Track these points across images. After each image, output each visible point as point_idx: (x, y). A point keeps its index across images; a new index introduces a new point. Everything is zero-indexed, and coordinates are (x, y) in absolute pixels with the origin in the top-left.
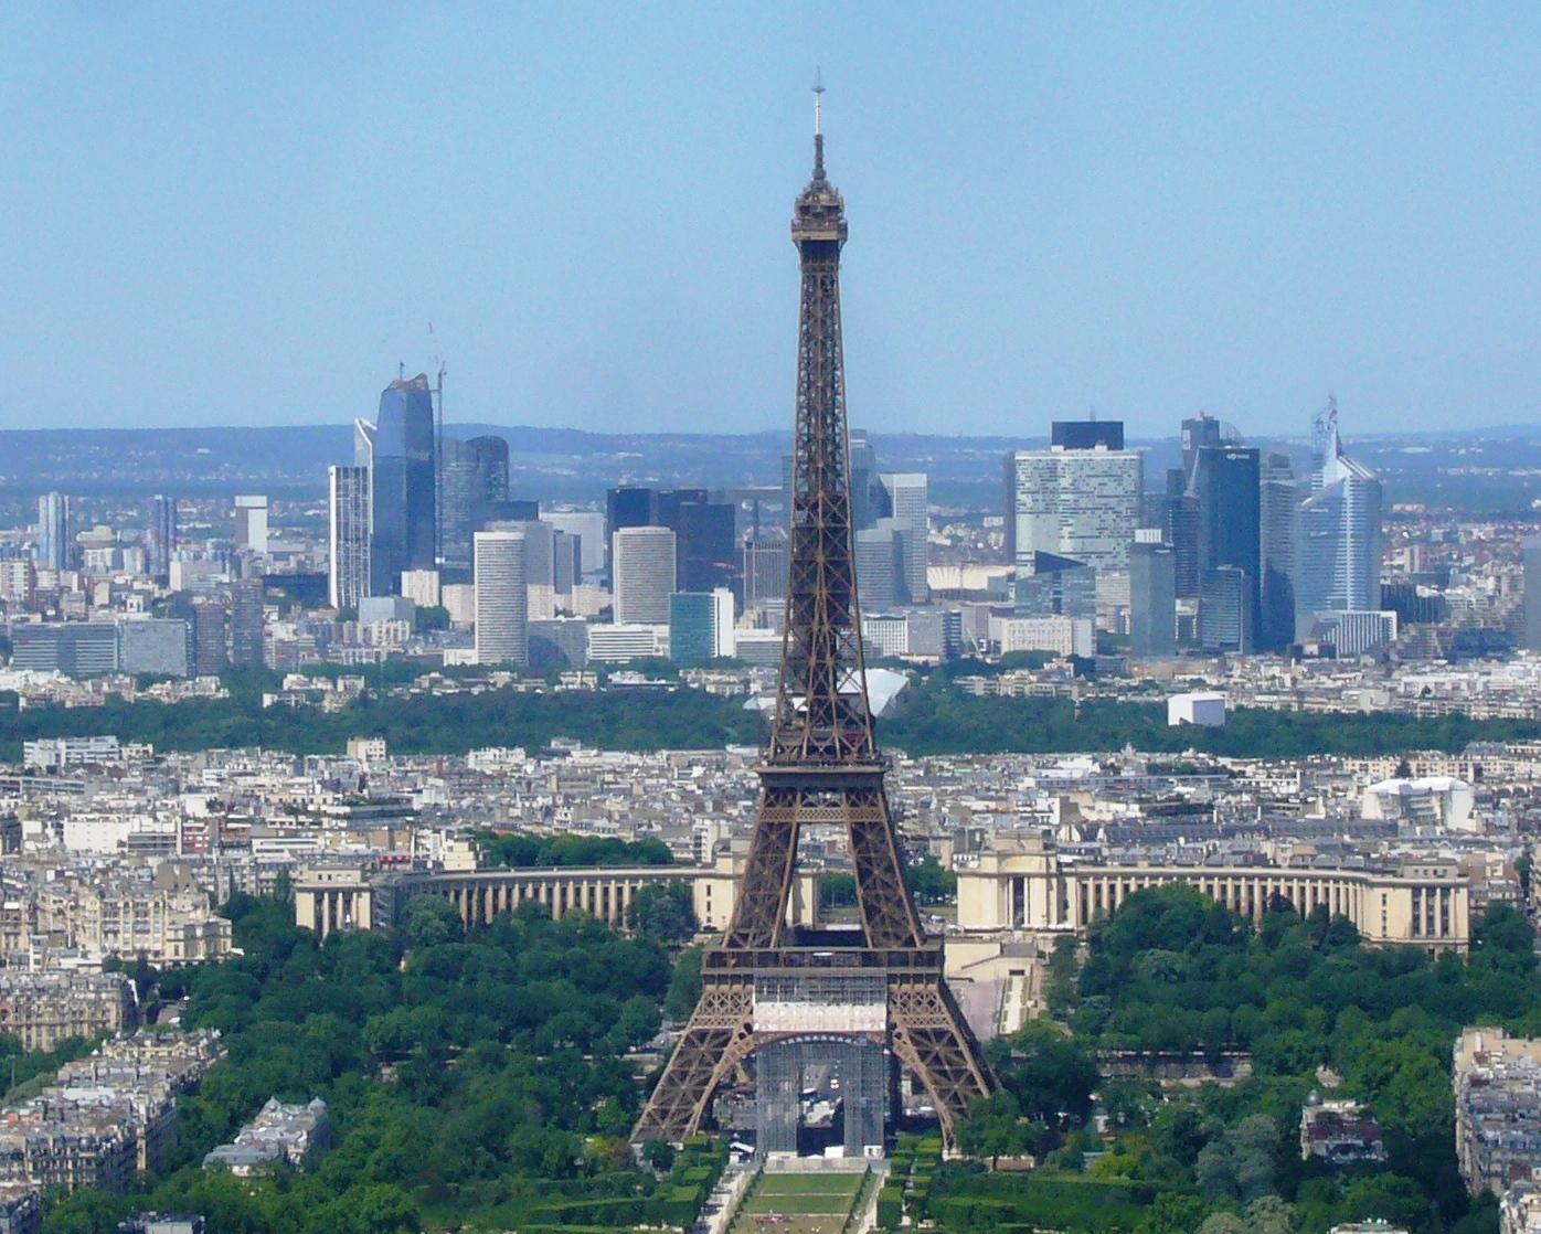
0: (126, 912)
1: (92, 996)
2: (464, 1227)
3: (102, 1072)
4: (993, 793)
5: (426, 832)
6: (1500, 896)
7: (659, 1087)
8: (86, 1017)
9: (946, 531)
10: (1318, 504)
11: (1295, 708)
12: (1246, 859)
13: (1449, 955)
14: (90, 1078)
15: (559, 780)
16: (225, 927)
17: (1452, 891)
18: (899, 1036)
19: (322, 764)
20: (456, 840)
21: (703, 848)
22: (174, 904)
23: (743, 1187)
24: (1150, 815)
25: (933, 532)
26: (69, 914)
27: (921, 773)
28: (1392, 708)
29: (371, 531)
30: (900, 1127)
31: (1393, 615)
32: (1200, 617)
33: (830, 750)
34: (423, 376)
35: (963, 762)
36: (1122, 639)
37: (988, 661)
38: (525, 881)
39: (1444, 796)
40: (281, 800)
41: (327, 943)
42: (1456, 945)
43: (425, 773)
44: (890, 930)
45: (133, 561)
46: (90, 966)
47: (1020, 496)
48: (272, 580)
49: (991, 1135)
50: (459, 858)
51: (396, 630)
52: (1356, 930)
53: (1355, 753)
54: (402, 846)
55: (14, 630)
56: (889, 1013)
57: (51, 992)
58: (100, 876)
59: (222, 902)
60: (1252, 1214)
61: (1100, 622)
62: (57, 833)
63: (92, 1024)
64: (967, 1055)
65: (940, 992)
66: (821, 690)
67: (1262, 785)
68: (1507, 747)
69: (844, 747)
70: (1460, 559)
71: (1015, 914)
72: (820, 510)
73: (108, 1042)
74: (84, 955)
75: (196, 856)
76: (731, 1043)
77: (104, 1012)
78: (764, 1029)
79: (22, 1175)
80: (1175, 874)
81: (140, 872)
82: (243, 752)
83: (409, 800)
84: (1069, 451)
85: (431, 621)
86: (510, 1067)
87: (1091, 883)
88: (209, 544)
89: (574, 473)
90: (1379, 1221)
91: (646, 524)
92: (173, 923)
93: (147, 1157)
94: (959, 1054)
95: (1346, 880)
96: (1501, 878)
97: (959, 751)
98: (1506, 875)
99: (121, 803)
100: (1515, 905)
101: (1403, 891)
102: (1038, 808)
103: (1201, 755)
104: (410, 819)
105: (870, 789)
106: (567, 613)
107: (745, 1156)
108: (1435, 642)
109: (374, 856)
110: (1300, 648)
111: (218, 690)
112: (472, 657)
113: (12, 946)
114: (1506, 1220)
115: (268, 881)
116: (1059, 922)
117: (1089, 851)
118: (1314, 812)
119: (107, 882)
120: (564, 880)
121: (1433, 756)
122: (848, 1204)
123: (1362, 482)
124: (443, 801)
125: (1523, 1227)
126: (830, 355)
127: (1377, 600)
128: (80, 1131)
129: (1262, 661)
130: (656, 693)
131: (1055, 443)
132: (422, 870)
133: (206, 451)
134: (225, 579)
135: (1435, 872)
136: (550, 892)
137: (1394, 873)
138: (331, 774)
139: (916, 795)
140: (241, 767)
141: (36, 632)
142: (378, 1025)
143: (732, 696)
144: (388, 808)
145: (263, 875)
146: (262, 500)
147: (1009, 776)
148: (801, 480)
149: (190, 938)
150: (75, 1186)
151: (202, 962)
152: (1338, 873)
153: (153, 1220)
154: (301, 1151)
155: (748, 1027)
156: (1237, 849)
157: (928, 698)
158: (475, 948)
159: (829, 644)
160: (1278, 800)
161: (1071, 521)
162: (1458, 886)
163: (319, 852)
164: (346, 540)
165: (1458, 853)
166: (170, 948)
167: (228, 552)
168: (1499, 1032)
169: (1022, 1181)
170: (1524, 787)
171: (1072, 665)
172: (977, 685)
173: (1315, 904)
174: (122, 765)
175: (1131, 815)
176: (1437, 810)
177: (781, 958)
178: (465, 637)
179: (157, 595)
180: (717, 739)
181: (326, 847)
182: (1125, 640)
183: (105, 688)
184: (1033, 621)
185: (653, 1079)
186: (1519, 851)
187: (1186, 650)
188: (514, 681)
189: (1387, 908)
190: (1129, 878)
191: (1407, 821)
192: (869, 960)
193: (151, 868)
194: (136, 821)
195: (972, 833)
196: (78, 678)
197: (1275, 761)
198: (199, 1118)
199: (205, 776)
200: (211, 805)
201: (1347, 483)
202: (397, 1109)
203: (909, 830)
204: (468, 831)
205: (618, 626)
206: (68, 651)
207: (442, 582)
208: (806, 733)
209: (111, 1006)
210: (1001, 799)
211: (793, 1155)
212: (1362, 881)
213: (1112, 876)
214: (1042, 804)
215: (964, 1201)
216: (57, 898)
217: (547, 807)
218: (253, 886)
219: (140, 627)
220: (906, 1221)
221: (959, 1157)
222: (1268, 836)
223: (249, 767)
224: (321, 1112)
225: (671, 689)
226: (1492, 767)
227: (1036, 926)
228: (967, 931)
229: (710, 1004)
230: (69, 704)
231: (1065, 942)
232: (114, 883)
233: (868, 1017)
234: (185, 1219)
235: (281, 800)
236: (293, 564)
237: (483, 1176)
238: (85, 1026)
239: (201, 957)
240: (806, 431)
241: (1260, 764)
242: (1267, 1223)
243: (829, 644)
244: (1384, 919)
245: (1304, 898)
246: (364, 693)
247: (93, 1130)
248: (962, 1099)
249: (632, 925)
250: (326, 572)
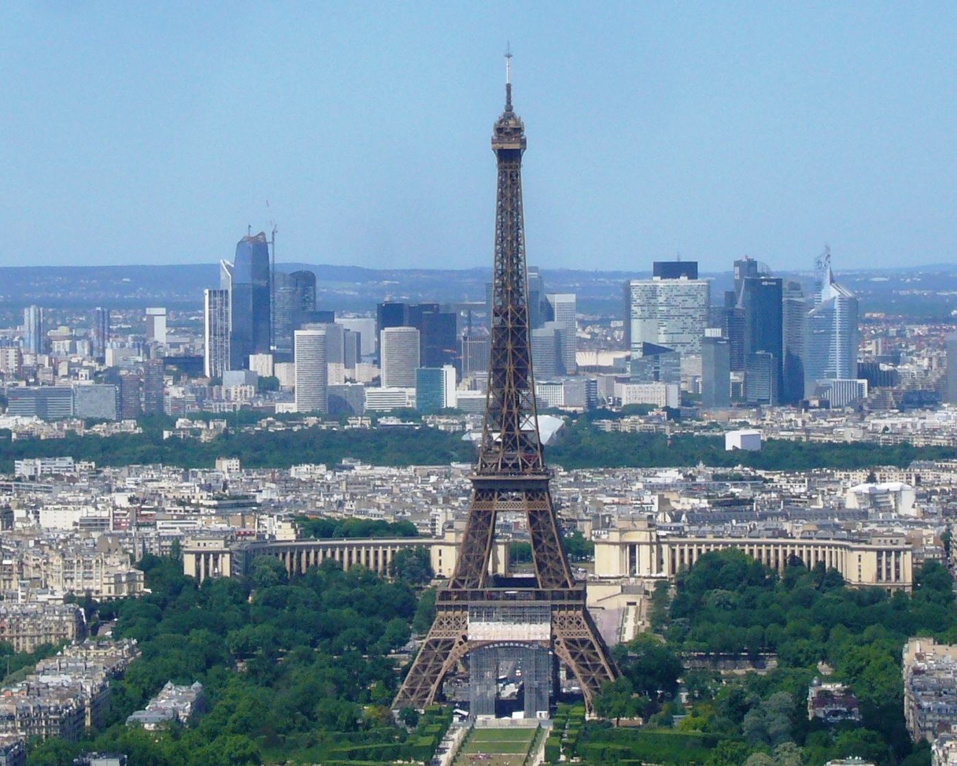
0: (78, 566)
1: (57, 618)
2: (288, 762)
3: (63, 665)
4: (616, 492)
5: (265, 517)
6: (931, 556)
7: (409, 675)
8: (53, 631)
9: (587, 330)
10: (819, 313)
11: (804, 440)
12: (774, 533)
13: (900, 593)
14: (56, 669)
15: (347, 484)
16: (140, 576)
17: (902, 553)
19: (200, 474)
20: (283, 522)
21: (437, 526)
22: (108, 561)
23: (462, 737)
25: (579, 330)
26: (43, 567)
27: (572, 480)
28: (864, 440)
29: (230, 330)
30: (559, 700)
31: (865, 382)
32: (745, 383)
33: (515, 466)
34: (262, 234)
36: (697, 396)
37: (614, 410)
38: (326, 547)
39: (897, 494)
40: (174, 497)
41: (203, 585)
42: (904, 586)
43: (264, 480)
44: (553, 577)
45: (83, 348)
46: (56, 599)
47: (633, 308)
48: (169, 360)
49: (616, 704)
50: (285, 533)
51: (246, 391)
52: (842, 578)
53: (841, 467)
54: (250, 525)
55: (8, 391)
56: (552, 629)
57: (32, 615)
58: (62, 544)
59: (138, 560)
60: (778, 753)
61: (683, 386)
62: (35, 517)
63: (57, 635)
64: (601, 655)
65: (584, 616)
66: (510, 428)
67: (784, 487)
68: (936, 464)
69: (524, 464)
71: (630, 567)
72: (509, 317)
73: (67, 647)
74: (52, 593)
75: (121, 531)
76: (454, 647)
77: (64, 628)
78: (474, 639)
79: (14, 730)
80: (730, 543)
81: (87, 541)
82: (151, 467)
83: (254, 497)
84: (664, 280)
85: (268, 385)
86: (317, 662)
87: (677, 548)
88: (130, 338)
89: (356, 293)
90: (857, 758)
91: (401, 325)
92: (107, 573)
93: (91, 718)
94: (596, 654)
95: (836, 546)
96: (932, 545)
98: (935, 543)
99: (75, 499)
100: (941, 562)
101: (871, 553)
102: (645, 502)
103: (746, 469)
104: (255, 508)
105: (540, 490)
106: (352, 380)
107: (463, 718)
108: (891, 398)
109: (232, 532)
110: (807, 402)
111: (135, 428)
112: (293, 408)
113: (7, 587)
114: (935, 757)
115: (166, 547)
116: (657, 573)
117: (677, 528)
118: (816, 504)
119: (66, 548)
120: (350, 546)
121: (890, 469)
122: (527, 747)
123: (846, 299)
124: (275, 497)
125: (946, 761)
126: (515, 220)
127: (855, 372)
128: (50, 702)
129: (784, 410)
130: (408, 430)
131: (655, 275)
132: (262, 540)
133: (128, 280)
134: (140, 359)
135: (891, 541)
136: (341, 554)
137: (866, 542)
138: (205, 481)
139: (569, 493)
140: (150, 476)
141: (23, 393)
143: (455, 432)
144: (241, 501)
145: (164, 543)
146: (163, 311)
147: (627, 482)
148: (497, 298)
149: (118, 583)
150: (47, 736)
151: (125, 597)
152: (831, 542)
153: (95, 757)
154: (187, 714)
155: (465, 638)
156: (768, 527)
157: (576, 433)
158: (295, 588)
159: (515, 400)
160: (793, 497)
161: (665, 323)
162: (905, 550)
164: (215, 335)
165: (905, 529)
166: (105, 589)
167: (142, 343)
168: (931, 641)
169: (635, 733)
170: (947, 488)
171: (666, 413)
172: (607, 425)
173: (817, 561)
174: (76, 475)
175: (702, 506)
176: (893, 503)
177: (485, 595)
178: (289, 395)
179: (97, 369)
180: (445, 459)
181: (203, 526)
182: (699, 397)
183: (65, 427)
184: (642, 386)
185: (406, 670)
186: (944, 528)
187: (737, 404)
188: (319, 423)
189: (861, 564)
190: (701, 545)
191: (874, 510)
192: (540, 596)
193: (94, 539)
194: (85, 510)
195: (604, 517)
196: (49, 421)
197: (792, 472)
198: (124, 694)
199: (127, 482)
200: (131, 500)
201: (837, 300)
203: (565, 516)
204: (291, 516)
205: (384, 388)
206: (42, 404)
207: (275, 362)
208: (501, 455)
209: (69, 624)
210: (622, 496)
211: (493, 717)
212: (846, 547)
213: (691, 544)
214: (647, 499)
215: (599, 746)
216: (35, 558)
217: (340, 501)
218: (157, 550)
219: (87, 389)
220: (563, 758)
221: (596, 718)
222: (787, 519)
223: (155, 476)
224: (200, 690)
225: (417, 428)
226: (927, 476)
227: (643, 575)
228: (600, 578)
229: (441, 623)
230: (43, 437)
231: (662, 585)
232: (71, 548)
233: (539, 631)
234: (115, 757)
235: (174, 497)
236: (182, 350)
237: (300, 730)
238: (53, 637)
239: (125, 594)
240: (500, 267)
241: (783, 474)
242: (787, 759)
244: (860, 570)
245: (810, 558)
246: (226, 430)
247: (58, 702)
248: (597, 682)
249: (392, 574)
250: (202, 355)
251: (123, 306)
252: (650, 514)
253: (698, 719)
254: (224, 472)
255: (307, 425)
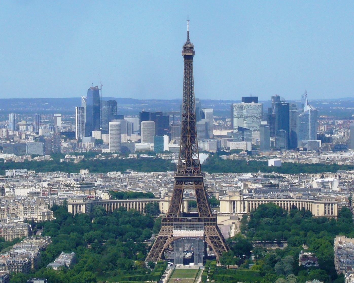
0: (29, 209)
1: (21, 228)
2: (107, 281)
3: (23, 246)
4: (228, 182)
5: (98, 191)
6: (345, 205)
7: (151, 249)
8: (20, 233)
9: (217, 122)
10: (303, 116)
11: (297, 162)
12: (286, 197)
13: (333, 219)
14: (21, 247)
15: (128, 179)
16: (52, 213)
17: (334, 204)
18: (206, 238)
19: (74, 175)
20: (105, 193)
21: (162, 194)
22: (40, 207)
23: (171, 272)
24: (264, 187)
25: (214, 122)
26: (16, 210)
27: (212, 177)
28: (320, 162)
29: (85, 122)
30: (207, 258)
31: (320, 141)
32: (276, 142)
33: (191, 172)
34: (97, 86)
35: (221, 175)
36: (258, 146)
37: (227, 152)
38: (121, 202)
39: (332, 183)
40: (64, 183)
41: (75, 216)
42: (335, 217)
43: (98, 177)
44: (204, 213)
45: (31, 129)
46: (21, 221)
47: (234, 114)
48: (63, 133)
49: (228, 260)
50: (105, 197)
51: (91, 145)
52: (312, 213)
53: (311, 173)
54: (92, 194)
55: (3, 145)
56: (204, 232)
57: (12, 227)
58: (23, 201)
59: (51, 207)
60: (288, 278)
61: (253, 143)
62: (13, 191)
63: (21, 235)
64: (222, 242)
65: (216, 227)
66: (189, 158)
67: (290, 180)
68: (346, 171)
69: (194, 171)
70: (335, 128)
71: (233, 210)
72: (188, 117)
73: (25, 239)
74: (19, 219)
75: (45, 196)
76: (168, 239)
77: (24, 232)
78: (175, 236)
79: (5, 270)
80: (270, 201)
81: (32, 200)
82: (56, 172)
83: (94, 184)
84: (246, 104)
85: (99, 142)
86: (117, 245)
87: (251, 202)
88: (48, 125)
89: (132, 108)
90: (317, 280)
91: (148, 120)
92: (40, 212)
93: (34, 265)
94: (220, 242)
95: (309, 202)
96: (345, 201)
97: (220, 172)
98: (346, 201)
99: (28, 184)
100: (348, 207)
101: (322, 204)
102: (239, 185)
103: (276, 173)
104: (94, 188)
105: (200, 181)
106: (130, 141)
107: (171, 265)
108: (330, 147)
109: (86, 196)
110: (299, 149)
111: (50, 158)
112: (108, 151)
113: (3, 217)
114: (346, 280)
115: (61, 202)
116: (243, 212)
117: (250, 195)
118: (302, 186)
119: (25, 202)
120: (130, 202)
121: (329, 173)
122: (195, 276)
123: (313, 111)
124: (102, 184)
125: (350, 281)
126: (191, 81)
127: (316, 138)
128: (18, 259)
129: (290, 152)
130: (151, 159)
131: (242, 102)
132: (97, 200)
133: (47, 103)
134: (52, 133)
135: (330, 200)
136: (126, 205)
137: (320, 200)
138: (76, 178)
139: (211, 182)
140: (55, 176)
141: (8, 145)
142: (87, 235)
143: (168, 160)
144: (89, 185)
145: (60, 201)
146: (60, 115)
147: (232, 178)
148: (184, 110)
149: (44, 215)
150: (17, 272)
151: (46, 221)
152: (307, 200)
153: (35, 280)
154: (69, 264)
155: (172, 236)
156: (284, 195)
157: (213, 160)
158: (109, 217)
159: (190, 148)
160: (294, 184)
161: (246, 120)
162: (335, 203)
163: (73, 195)
164: (80, 124)
165: (335, 196)
166: (39, 217)
167: (52, 127)
168: (344, 237)
169: (235, 271)
170: (350, 180)
171: (246, 153)
172: (225, 157)
173: (302, 207)
174: (28, 175)
175: (260, 187)
176: (330, 186)
177: (179, 220)
178: (107, 146)
179: (36, 137)
182: (258, 147)
183: (24, 158)
184: (237, 142)
185: (150, 248)
186: (349, 195)
187: (272, 149)
188: (118, 156)
189: (319, 208)
190: (259, 201)
191: (323, 188)
192: (200, 220)
193: (35, 199)
194: (31, 188)
195: (223, 191)
196: (18, 156)
197: (293, 175)
198: (46, 256)
199: (47, 178)
200: (48, 185)
201: (310, 111)
202: (91, 254)
203: (209, 190)
204: (108, 190)
205: (142, 144)
206: (16, 149)
207: (102, 134)
208: (185, 168)
209: (26, 231)
210: (230, 183)
211: (182, 265)
212: (313, 202)
213: (255, 201)
214: (239, 184)
215: (221, 275)
216: (13, 206)
217: (126, 185)
218: (58, 203)
219: (32, 144)
220: (208, 280)
221: (220, 265)
222: (291, 192)
223: (57, 176)
224: (74, 255)
225: (154, 158)
227: (238, 212)
228: (222, 213)
229: (163, 230)
230: (16, 162)
231: (245, 216)
232: (26, 203)
233: (199, 233)
234: (42, 280)
235: (64, 183)
236: (67, 129)
237: (111, 270)
238: (20, 235)
239: (46, 219)
240: (185, 99)
241: (290, 175)
242: (291, 280)
243: (190, 148)
244: (318, 211)
245: (300, 206)
246: (84, 159)
247: (21, 259)
248: (221, 252)
249: (145, 212)
250: (75, 131)
251: (45, 113)
252: (240, 190)
253: (258, 266)
254: (83, 174)
255: (113, 157)
